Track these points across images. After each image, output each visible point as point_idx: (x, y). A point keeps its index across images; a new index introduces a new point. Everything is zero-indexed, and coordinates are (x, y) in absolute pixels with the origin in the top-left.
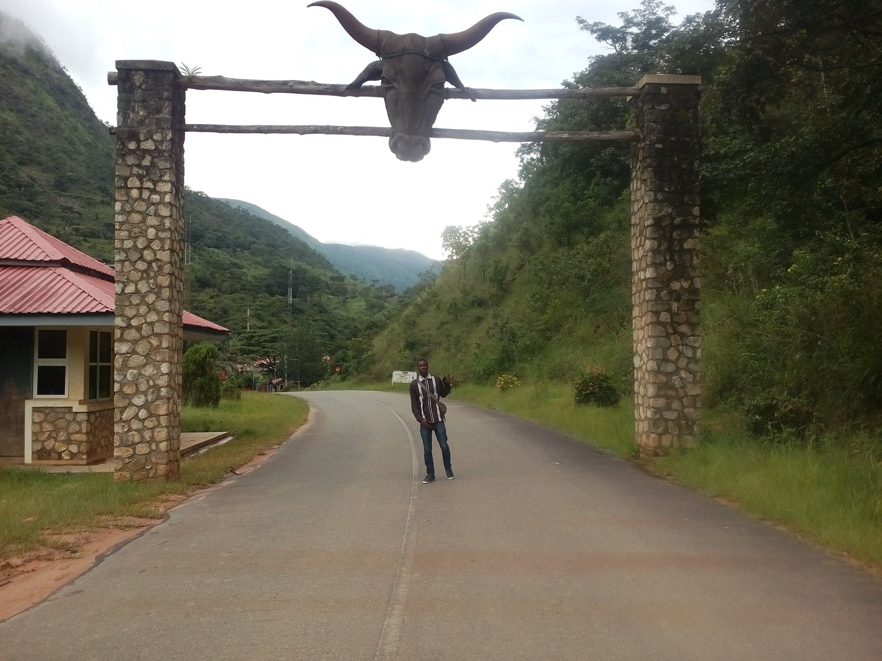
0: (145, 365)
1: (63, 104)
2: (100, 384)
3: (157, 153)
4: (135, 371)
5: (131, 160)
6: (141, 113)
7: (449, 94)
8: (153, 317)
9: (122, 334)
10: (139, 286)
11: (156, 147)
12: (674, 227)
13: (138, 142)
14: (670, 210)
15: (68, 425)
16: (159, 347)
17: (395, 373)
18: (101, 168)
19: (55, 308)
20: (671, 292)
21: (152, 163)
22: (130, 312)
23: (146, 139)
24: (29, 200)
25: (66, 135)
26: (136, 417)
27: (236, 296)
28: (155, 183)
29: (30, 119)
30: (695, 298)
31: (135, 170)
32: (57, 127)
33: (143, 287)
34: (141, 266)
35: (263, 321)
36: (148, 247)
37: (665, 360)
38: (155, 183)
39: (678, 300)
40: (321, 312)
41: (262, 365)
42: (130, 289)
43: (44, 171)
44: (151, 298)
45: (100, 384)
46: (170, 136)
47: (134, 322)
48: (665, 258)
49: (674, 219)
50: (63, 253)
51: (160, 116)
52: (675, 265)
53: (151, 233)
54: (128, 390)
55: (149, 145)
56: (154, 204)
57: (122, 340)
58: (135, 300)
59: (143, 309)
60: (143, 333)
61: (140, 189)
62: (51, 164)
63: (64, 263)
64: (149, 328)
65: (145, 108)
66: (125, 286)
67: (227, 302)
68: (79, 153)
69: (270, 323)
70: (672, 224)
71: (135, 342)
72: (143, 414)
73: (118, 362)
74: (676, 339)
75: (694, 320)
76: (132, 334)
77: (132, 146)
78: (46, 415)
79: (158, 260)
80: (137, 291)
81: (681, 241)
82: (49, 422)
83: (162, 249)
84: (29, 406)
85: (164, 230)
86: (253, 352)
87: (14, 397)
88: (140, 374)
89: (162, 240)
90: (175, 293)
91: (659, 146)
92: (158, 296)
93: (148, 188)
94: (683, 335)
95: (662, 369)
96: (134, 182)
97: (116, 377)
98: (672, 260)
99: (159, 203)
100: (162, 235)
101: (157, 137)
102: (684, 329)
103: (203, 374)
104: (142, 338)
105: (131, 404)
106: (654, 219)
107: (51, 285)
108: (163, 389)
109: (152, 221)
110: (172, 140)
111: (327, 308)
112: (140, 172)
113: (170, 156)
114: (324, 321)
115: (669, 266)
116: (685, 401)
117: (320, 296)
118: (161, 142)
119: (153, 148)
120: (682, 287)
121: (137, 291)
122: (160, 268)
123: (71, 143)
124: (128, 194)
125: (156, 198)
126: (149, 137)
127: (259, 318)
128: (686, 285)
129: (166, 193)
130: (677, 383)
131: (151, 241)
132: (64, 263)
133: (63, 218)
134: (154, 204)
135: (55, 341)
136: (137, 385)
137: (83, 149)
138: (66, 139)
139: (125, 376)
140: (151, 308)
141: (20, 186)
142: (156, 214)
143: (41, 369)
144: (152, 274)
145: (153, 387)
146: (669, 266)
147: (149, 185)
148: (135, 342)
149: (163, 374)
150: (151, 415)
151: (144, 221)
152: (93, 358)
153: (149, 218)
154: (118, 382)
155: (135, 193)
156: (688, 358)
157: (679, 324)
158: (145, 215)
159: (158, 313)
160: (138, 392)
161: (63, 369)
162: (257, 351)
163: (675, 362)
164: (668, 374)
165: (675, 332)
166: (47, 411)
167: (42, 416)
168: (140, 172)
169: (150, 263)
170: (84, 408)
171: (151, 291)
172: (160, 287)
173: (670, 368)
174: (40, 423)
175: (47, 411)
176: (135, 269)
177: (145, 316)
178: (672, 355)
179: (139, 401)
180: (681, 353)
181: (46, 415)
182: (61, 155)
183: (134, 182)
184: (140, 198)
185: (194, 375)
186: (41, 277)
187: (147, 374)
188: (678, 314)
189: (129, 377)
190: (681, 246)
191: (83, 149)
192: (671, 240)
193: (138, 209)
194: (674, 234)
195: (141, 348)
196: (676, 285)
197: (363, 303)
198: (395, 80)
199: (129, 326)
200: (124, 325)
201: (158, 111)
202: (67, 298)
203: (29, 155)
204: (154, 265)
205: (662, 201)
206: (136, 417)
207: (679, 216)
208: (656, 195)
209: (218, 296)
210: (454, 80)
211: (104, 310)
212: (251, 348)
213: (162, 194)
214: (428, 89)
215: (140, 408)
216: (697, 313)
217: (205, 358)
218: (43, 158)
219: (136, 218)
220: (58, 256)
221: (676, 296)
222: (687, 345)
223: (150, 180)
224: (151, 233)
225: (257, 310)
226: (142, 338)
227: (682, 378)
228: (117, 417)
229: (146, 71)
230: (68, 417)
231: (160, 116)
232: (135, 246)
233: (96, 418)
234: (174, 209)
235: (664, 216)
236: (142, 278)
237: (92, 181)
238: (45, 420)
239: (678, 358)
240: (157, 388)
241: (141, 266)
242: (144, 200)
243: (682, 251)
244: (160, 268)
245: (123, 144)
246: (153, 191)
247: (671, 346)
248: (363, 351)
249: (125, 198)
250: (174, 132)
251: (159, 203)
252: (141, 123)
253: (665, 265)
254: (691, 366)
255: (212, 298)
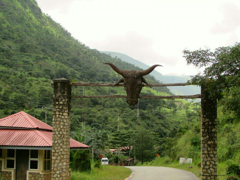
0: (59, 163)
1: (26, 6)
2: (48, 166)
3: (63, 105)
4: (57, 164)
5: (57, 107)
6: (60, 94)
7: (143, 86)
8: (62, 150)
9: (54, 154)
10: (58, 141)
11: (63, 103)
12: (209, 125)
13: (59, 102)
14: (208, 120)
15: (38, 178)
16: (63, 158)
17: (181, 158)
18: (43, 39)
19: (36, 145)
20: (208, 144)
21: (62, 107)
22: (56, 148)
23: (61, 101)
24: (7, 58)
25: (27, 22)
26: (57, 177)
27: (113, 109)
28: (63, 113)
29: (9, 15)
30: (215, 146)
31: (58, 110)
32: (22, 19)
33: (59, 141)
34: (59, 136)
35: (127, 124)
36: (61, 130)
37: (206, 165)
38: (63, 113)
39: (210, 147)
40: (159, 118)
41: (123, 150)
42: (56, 142)
43: (15, 42)
44: (61, 144)
45: (48, 166)
46: (67, 100)
47: (57, 151)
48: (206, 134)
49: (209, 123)
50: (38, 125)
51: (64, 95)
52: (209, 136)
53: (62, 127)
54: (55, 169)
55: (61, 103)
56: (62, 119)
57: (54, 156)
58: (57, 145)
59: (59, 148)
60: (59, 154)
61: (59, 115)
62: (18, 38)
63: (38, 129)
64: (61, 153)
65: (60, 92)
66: (55, 141)
67: (107, 113)
68: (33, 32)
69: (131, 125)
70: (208, 124)
71: (57, 156)
72: (59, 176)
73: (53, 162)
74: (209, 159)
75: (215, 153)
76: (56, 154)
77: (57, 103)
78: (33, 175)
79: (63, 134)
80: (58, 143)
81: (211, 129)
82: (33, 177)
83: (64, 131)
84: (28, 172)
85: (65, 126)
86: (118, 143)
87: (23, 169)
88: (58, 165)
89: (64, 129)
90: (68, 143)
91: (205, 101)
92: (63, 144)
93: (61, 115)
94: (211, 157)
95: (205, 167)
96: (57, 113)
97: (52, 166)
98: (208, 135)
99: (64, 119)
100: (64, 127)
101: (64, 100)
102: (212, 155)
103: (84, 160)
104: (59, 155)
105: (56, 173)
106: (203, 122)
107: (34, 137)
108: (64, 170)
109: (62, 123)
110: (67, 101)
111: (164, 116)
112: (59, 110)
113: (67, 106)
114: (162, 124)
115: (207, 137)
116: (212, 177)
117: (160, 109)
118: (65, 102)
119: (62, 103)
120: (211, 143)
121: (58, 143)
122: (64, 136)
123: (29, 27)
124: (56, 116)
125: (63, 117)
126: (61, 100)
127: (125, 122)
128: (212, 142)
129: (65, 116)
130: (209, 172)
131: (61, 129)
132: (38, 129)
133: (24, 67)
134: (62, 119)
135: (35, 153)
136: (57, 168)
137: (35, 30)
138: (26, 25)
139: (54, 165)
140: (61, 147)
141: (3, 51)
142: (63, 122)
143: (31, 161)
144: (62, 138)
145: (61, 169)
146: (207, 137)
147: (61, 114)
148: (57, 156)
149: (64, 165)
150: (61, 176)
151: (60, 123)
152: (45, 158)
153: (61, 123)
154: (53, 167)
155: (58, 116)
156: (213, 164)
157: (210, 154)
158: (60, 122)
159: (63, 148)
160: (58, 170)
161: (37, 161)
162: (120, 143)
163: (209, 165)
164: (207, 169)
165: (209, 156)
166: (33, 174)
167: (31, 175)
168: (59, 110)
169: (61, 135)
170: (43, 173)
171: (61, 142)
172: (64, 142)
173: (207, 167)
174: (31, 177)
175: (33, 174)
176: (57, 137)
177: (59, 149)
178: (208, 163)
179: (58, 172)
180: (211, 163)
181: (33, 175)
182: (24, 33)
183: (57, 113)
184: (59, 117)
185: (80, 160)
186: (32, 133)
187: (60, 165)
188: (210, 151)
189: (55, 166)
190: (211, 130)
191: (35, 30)
192: (208, 129)
193: (58, 120)
194: (209, 127)
195: (59, 158)
196: (209, 143)
197: (185, 113)
198: (127, 84)
199: (56, 152)
200: (54, 152)
201: (64, 93)
202: (39, 141)
203: (8, 34)
204: (62, 135)
205: (205, 117)
206: (57, 177)
207: (210, 121)
208: (203, 116)
209: (102, 109)
210: (145, 82)
211: (49, 146)
212: (117, 141)
213: (65, 116)
214: (136, 86)
215: (58, 174)
216: (216, 151)
217: (85, 153)
218: (15, 35)
219: (58, 122)
220: (36, 127)
221: (209, 146)
222: (212, 160)
223: (62, 112)
224: (62, 127)
225: (123, 117)
226: (59, 155)
227: (211, 170)
228: (52, 176)
229: (61, 83)
230: (39, 176)
231: (64, 95)
232: (57, 130)
233: (46, 176)
234: (68, 120)
235: (206, 122)
236: (59, 139)
237: (38, 47)
238: (32, 176)
239: (210, 164)
240: (62, 169)
241: (59, 136)
242: (60, 118)
243: (211, 132)
244: (64, 136)
245: (55, 102)
246: (62, 115)
247: (208, 161)
248: (172, 146)
249: (55, 117)
250: (68, 99)
251: (64, 119)
252: (59, 97)
253: (206, 136)
254: (214, 167)
255: (99, 111)
